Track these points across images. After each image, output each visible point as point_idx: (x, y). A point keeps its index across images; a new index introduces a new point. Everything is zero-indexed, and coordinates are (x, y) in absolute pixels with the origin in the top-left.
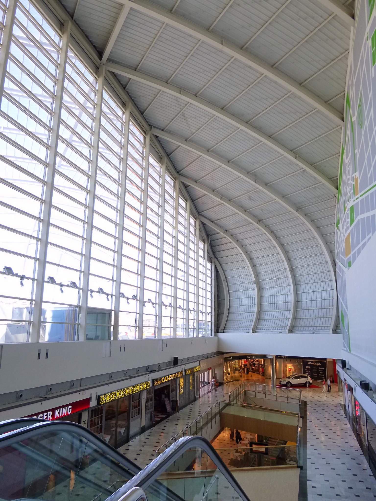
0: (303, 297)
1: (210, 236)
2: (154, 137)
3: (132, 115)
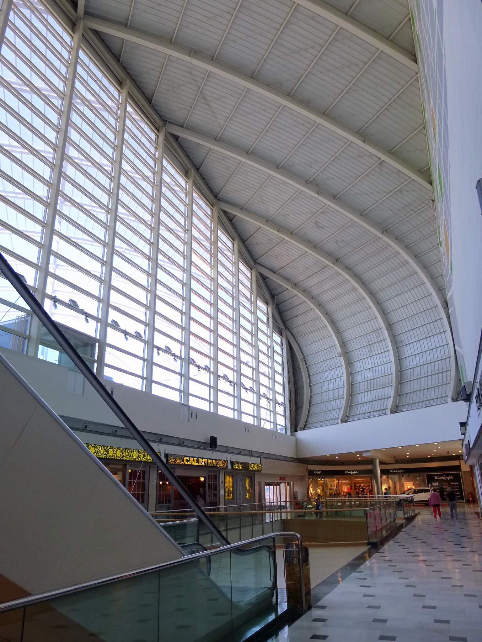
0: (408, 363)
1: (275, 297)
2: (171, 135)
3: (130, 95)
